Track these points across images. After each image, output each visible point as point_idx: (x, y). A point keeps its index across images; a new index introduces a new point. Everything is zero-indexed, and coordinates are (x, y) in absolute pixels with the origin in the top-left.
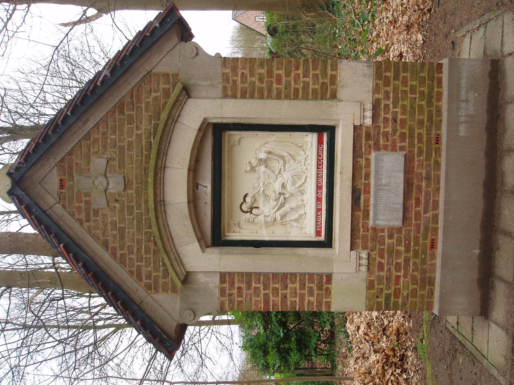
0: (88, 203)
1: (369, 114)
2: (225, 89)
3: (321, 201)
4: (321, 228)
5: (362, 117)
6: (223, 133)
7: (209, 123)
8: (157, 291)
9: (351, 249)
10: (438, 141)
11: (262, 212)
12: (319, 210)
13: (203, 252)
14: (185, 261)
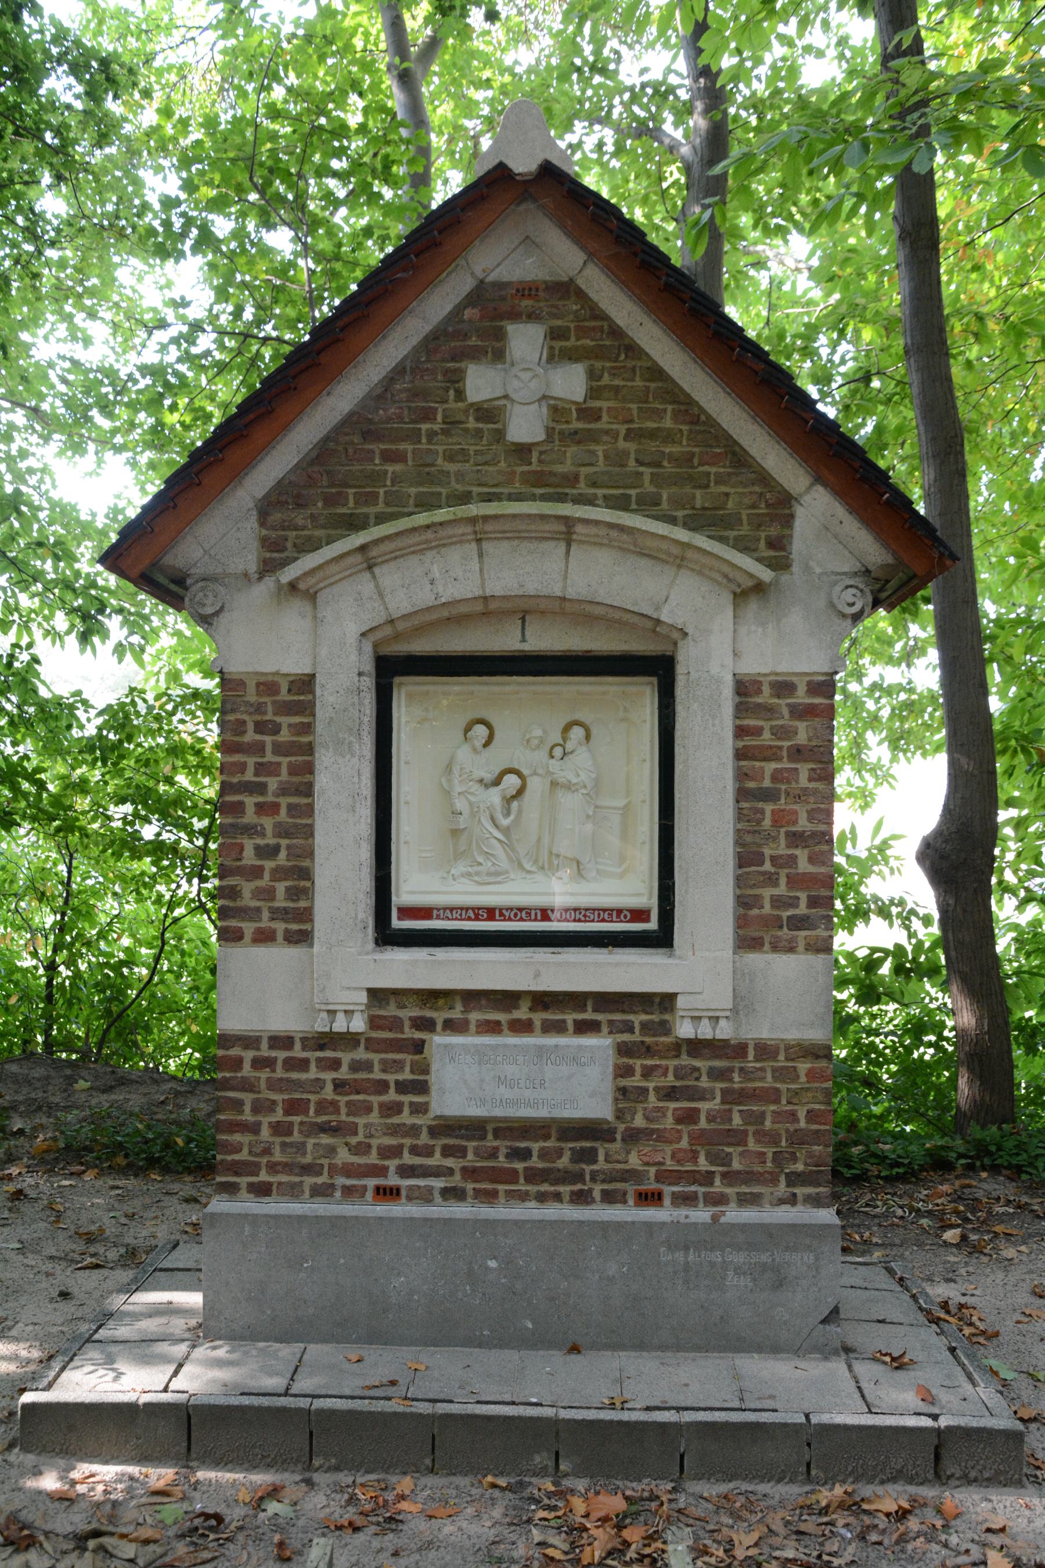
1: (705, 1031)
3: (632, 920)
4: (438, 918)
5: (697, 1014)
6: (654, 680)
7: (675, 644)
10: (391, 1194)
11: (885, 777)
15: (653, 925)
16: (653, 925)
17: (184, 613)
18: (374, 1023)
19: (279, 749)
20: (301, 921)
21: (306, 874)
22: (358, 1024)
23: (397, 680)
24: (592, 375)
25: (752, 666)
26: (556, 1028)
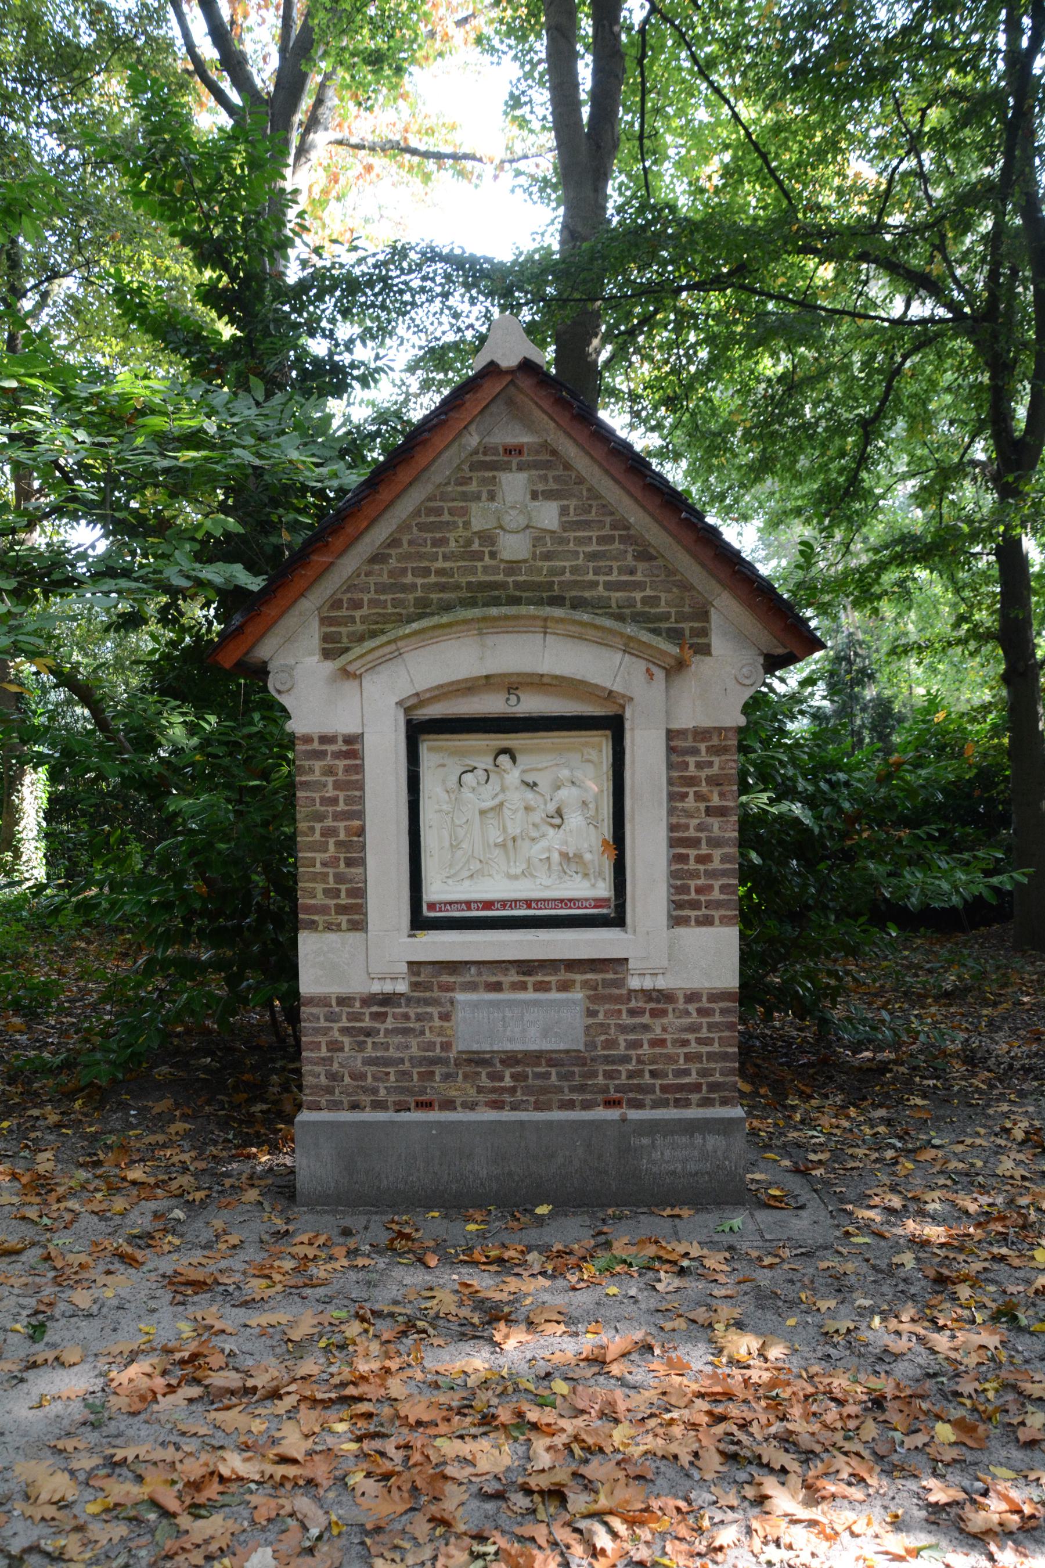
0: (477, 498)
1: (648, 984)
2: (680, 733)
6: (608, 733)
7: (623, 707)
8: (324, 621)
9: (410, 963)
13: (399, 704)
17: (265, 651)
18: (415, 986)
20: (356, 897)
22: (402, 987)
24: (564, 511)
26: (542, 987)
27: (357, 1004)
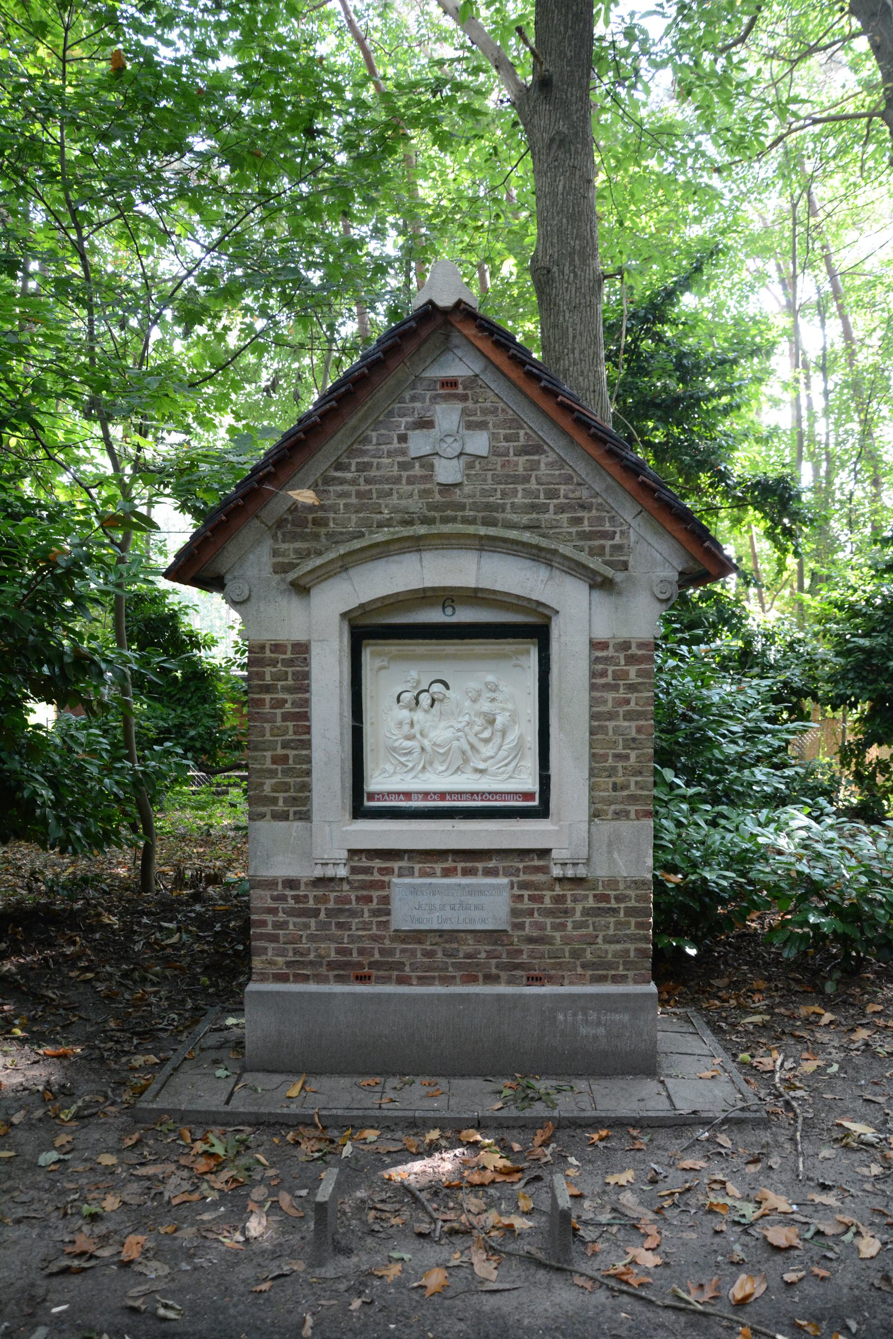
2: (604, 646)
7: (550, 618)
12: (408, 795)
13: (344, 615)
14: (326, 585)
15: (536, 803)
16: (536, 803)
18: (354, 870)
19: (286, 717)
21: (306, 716)
23: (365, 642)
25: (602, 633)
27: (280, 887)
